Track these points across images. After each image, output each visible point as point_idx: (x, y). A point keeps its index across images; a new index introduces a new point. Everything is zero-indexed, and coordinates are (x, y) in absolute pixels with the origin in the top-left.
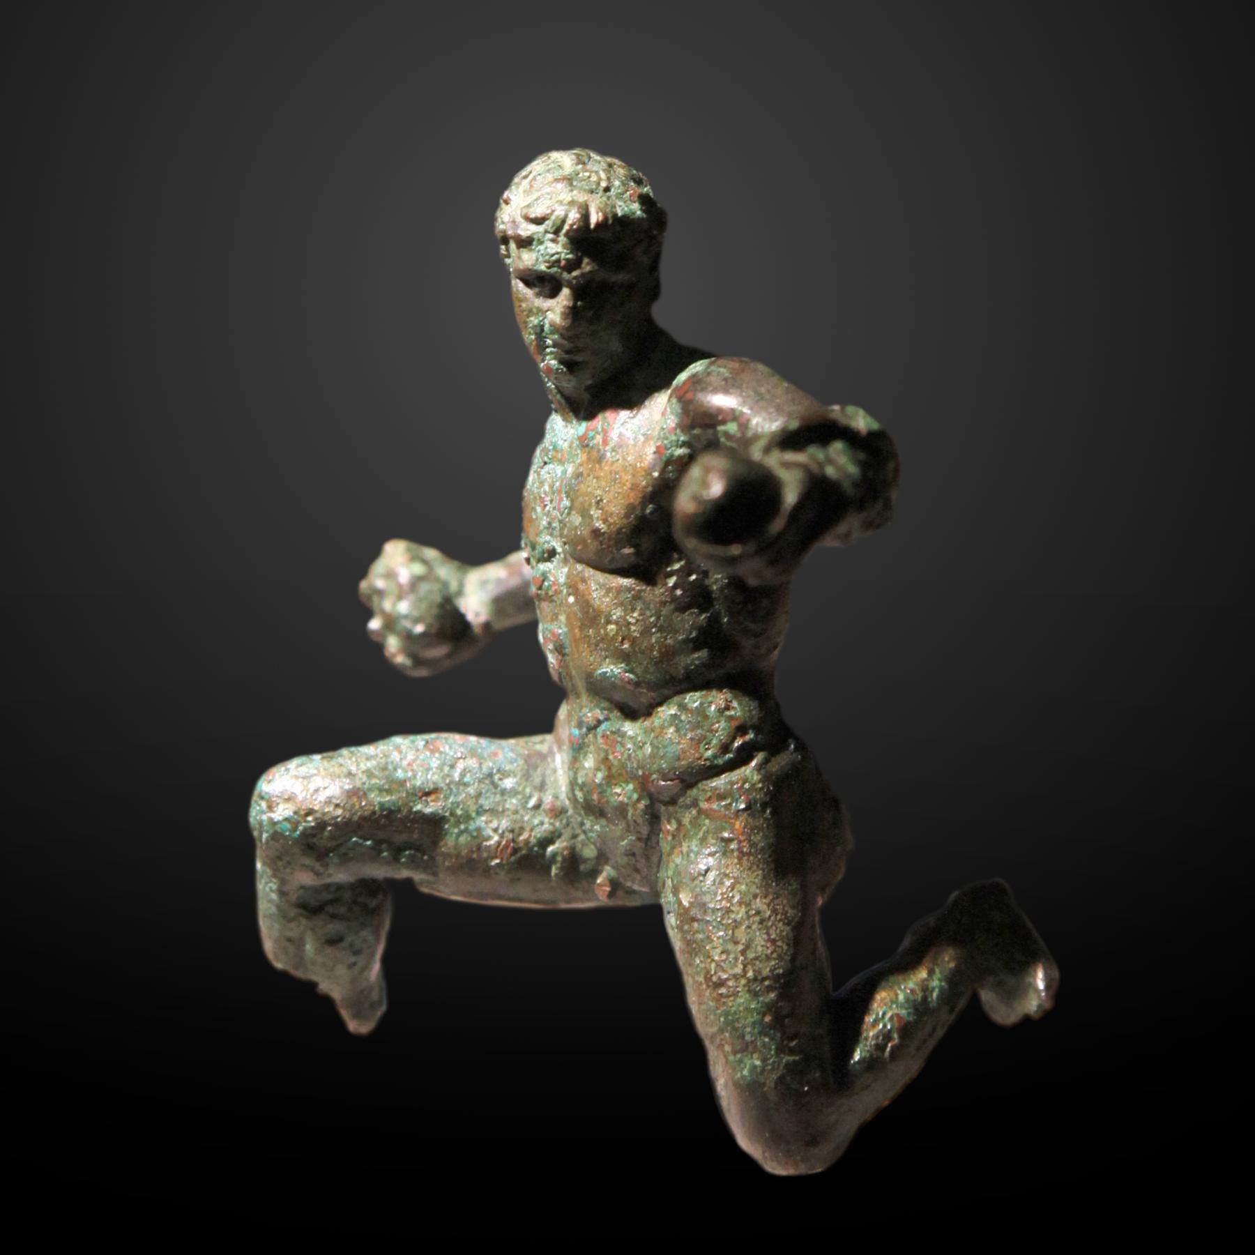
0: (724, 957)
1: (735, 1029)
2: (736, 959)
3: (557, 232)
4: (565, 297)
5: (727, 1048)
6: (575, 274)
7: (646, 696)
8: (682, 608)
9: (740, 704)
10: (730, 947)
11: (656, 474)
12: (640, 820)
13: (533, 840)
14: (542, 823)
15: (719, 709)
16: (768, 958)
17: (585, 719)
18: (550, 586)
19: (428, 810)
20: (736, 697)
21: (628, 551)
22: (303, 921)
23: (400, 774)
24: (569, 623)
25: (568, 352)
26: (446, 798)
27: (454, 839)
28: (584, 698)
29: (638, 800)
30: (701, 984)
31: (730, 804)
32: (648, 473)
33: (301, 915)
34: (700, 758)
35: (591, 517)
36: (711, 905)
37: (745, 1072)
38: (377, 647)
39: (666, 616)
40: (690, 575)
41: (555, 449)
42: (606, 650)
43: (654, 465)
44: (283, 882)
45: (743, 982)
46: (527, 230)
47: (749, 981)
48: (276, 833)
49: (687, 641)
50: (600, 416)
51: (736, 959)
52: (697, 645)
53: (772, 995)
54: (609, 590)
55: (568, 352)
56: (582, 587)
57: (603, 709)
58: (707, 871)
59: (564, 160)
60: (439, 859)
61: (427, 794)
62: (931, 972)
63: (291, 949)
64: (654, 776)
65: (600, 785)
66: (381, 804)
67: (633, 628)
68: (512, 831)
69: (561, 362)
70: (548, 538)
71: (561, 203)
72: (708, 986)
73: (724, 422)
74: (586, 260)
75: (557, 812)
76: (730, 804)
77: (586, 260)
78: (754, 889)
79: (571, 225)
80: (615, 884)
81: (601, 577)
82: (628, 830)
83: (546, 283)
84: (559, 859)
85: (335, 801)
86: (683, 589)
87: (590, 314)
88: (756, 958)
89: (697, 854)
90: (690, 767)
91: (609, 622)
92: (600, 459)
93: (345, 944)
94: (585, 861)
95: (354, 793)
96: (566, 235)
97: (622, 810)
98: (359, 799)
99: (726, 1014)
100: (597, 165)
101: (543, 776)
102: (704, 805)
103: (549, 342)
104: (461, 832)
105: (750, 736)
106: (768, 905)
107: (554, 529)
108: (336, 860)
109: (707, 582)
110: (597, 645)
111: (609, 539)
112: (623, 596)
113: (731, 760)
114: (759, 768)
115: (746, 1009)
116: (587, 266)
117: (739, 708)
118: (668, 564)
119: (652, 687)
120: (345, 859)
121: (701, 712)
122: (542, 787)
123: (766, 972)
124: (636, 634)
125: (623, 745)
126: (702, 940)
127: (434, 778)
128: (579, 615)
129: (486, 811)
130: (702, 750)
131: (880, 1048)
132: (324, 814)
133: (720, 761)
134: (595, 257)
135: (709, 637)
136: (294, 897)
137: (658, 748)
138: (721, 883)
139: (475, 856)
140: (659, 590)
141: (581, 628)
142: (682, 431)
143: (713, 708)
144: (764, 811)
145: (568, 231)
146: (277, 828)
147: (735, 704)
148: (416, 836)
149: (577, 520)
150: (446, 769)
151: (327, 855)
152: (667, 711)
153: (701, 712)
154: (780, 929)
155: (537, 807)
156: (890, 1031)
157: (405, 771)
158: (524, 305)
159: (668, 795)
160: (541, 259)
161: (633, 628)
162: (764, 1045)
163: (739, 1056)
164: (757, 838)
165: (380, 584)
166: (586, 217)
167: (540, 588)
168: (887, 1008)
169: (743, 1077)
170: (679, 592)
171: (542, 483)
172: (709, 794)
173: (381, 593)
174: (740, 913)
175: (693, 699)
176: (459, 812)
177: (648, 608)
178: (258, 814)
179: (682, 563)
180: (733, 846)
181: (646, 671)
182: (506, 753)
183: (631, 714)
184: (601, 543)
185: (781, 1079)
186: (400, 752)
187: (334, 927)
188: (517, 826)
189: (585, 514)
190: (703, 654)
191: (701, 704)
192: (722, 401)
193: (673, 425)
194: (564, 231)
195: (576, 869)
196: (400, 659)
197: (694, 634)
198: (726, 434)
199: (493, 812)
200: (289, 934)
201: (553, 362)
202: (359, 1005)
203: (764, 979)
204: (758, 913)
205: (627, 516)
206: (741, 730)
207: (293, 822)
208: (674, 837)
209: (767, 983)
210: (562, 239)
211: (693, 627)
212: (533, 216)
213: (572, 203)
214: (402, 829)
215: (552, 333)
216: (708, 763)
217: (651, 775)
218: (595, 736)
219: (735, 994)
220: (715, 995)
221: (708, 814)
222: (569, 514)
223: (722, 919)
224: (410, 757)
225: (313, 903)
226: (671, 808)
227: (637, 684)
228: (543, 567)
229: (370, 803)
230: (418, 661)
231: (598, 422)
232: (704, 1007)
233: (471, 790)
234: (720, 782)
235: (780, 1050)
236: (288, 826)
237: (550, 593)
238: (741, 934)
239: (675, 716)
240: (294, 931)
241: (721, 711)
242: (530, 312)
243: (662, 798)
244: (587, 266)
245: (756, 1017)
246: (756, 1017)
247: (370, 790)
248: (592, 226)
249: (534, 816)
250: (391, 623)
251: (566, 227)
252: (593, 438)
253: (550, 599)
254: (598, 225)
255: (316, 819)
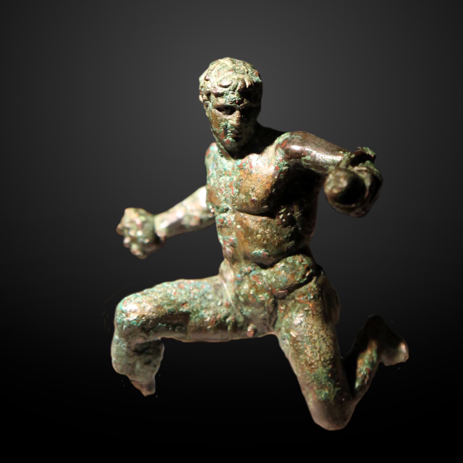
0: (312, 354)
1: (318, 380)
2: (317, 354)
3: (234, 90)
4: (237, 114)
5: (315, 388)
6: (241, 105)
7: (273, 259)
8: (285, 226)
9: (306, 259)
10: (314, 350)
11: (276, 177)
12: (270, 306)
13: (222, 317)
14: (224, 311)
15: (299, 261)
16: (328, 353)
17: (243, 270)
18: (227, 222)
19: (184, 310)
20: (304, 257)
21: (266, 207)
22: (136, 357)
23: (173, 298)
24: (237, 235)
25: (237, 134)
26: (190, 305)
27: (194, 320)
28: (243, 263)
29: (270, 299)
30: (303, 365)
31: (307, 297)
32: (273, 176)
33: (135, 355)
34: (295, 281)
35: (250, 196)
36: (305, 335)
37: (323, 396)
38: (128, 250)
39: (280, 230)
40: (287, 213)
41: (225, 170)
42: (256, 244)
43: (275, 174)
44: (129, 343)
45: (320, 362)
46: (220, 90)
47: (322, 362)
48: (130, 325)
49: (287, 238)
50: (247, 157)
51: (317, 354)
52: (290, 239)
53: (330, 366)
54: (257, 222)
55: (237, 134)
56: (244, 221)
57: (252, 266)
58: (301, 322)
59: (226, 62)
60: (188, 328)
61: (183, 304)
62: (372, 352)
63: (130, 368)
64: (277, 290)
65: (253, 295)
66: (169, 310)
67: (267, 235)
68: (214, 315)
69: (233, 138)
70: (225, 204)
71: (234, 79)
72: (307, 366)
73: (304, 156)
74: (245, 100)
75: (228, 306)
76: (307, 297)
77: (245, 100)
78: (319, 328)
79: (240, 87)
80: (255, 331)
81: (253, 217)
82: (265, 310)
83: (228, 110)
84: (231, 323)
85: (152, 311)
86: (285, 219)
87: (246, 119)
88: (324, 353)
89: (295, 317)
90: (292, 284)
91: (257, 234)
92: (250, 173)
93: (152, 364)
94: (240, 323)
95: (159, 307)
96: (238, 91)
97: (262, 303)
98: (161, 309)
99: (315, 375)
100: (241, 65)
101: (222, 293)
102: (297, 298)
103: (229, 131)
104: (196, 317)
105: (311, 271)
106: (325, 333)
107: (228, 200)
108: (153, 333)
109: (294, 215)
110: (252, 243)
111: (259, 203)
112: (263, 224)
113: (306, 281)
114: (316, 282)
115: (322, 373)
116: (245, 102)
117: (306, 262)
118: (280, 210)
119: (275, 256)
120: (156, 332)
121: (293, 263)
122: (222, 297)
123: (328, 358)
124: (269, 237)
125: (262, 279)
126: (303, 349)
127: (185, 298)
128: (244, 232)
129: (204, 308)
130: (295, 278)
131: (363, 381)
132: (149, 316)
133: (302, 282)
134: (248, 99)
135: (295, 236)
136: (133, 348)
137: (278, 279)
138: (307, 327)
139: (202, 326)
140: (276, 220)
141: (245, 237)
142: (286, 160)
143: (297, 262)
144: (319, 298)
145: (239, 90)
146: (131, 323)
147: (304, 260)
148: (180, 320)
149: (243, 197)
150: (188, 294)
151: (149, 331)
152: (280, 265)
153: (293, 263)
154: (329, 342)
155: (221, 305)
156: (366, 374)
157: (174, 296)
158: (219, 118)
159: (281, 297)
160: (227, 101)
161: (267, 235)
162: (329, 385)
163: (320, 390)
164: (318, 309)
165: (128, 225)
166: (245, 84)
167: (223, 223)
168: (364, 365)
169: (322, 398)
170: (284, 220)
171: (220, 184)
172: (299, 294)
173: (128, 229)
174: (316, 337)
175: (290, 259)
176: (195, 310)
177: (273, 227)
178: (118, 318)
179: (285, 209)
180: (310, 312)
181: (273, 250)
182: (205, 284)
183: (264, 267)
184: (255, 205)
185: (335, 398)
186: (170, 289)
187: (148, 358)
188: (215, 313)
189: (247, 194)
190: (293, 242)
191: (293, 261)
192: (296, 148)
193: (282, 158)
194: (237, 89)
195: (236, 327)
196: (138, 253)
197: (290, 235)
198: (306, 160)
199: (207, 308)
200: (130, 362)
201: (231, 139)
202: (149, 387)
203: (327, 361)
204: (322, 336)
205: (265, 194)
206: (308, 269)
207: (137, 320)
208: (284, 311)
209: (328, 362)
210: (236, 93)
211: (289, 233)
212: (224, 85)
213: (238, 79)
214: (175, 318)
215: (231, 128)
216: (298, 283)
217: (275, 288)
218: (249, 277)
219: (318, 368)
220: (310, 369)
221: (299, 302)
222: (238, 195)
223: (310, 340)
224: (174, 291)
225: (140, 349)
226: (283, 301)
227: (269, 256)
228: (224, 215)
229: (165, 310)
230: (144, 252)
231: (246, 159)
232: (304, 374)
233: (198, 301)
234: (303, 289)
235: (335, 386)
236: (135, 322)
237: (227, 225)
238: (317, 345)
239: (284, 267)
240: (131, 361)
241: (300, 263)
242: (221, 121)
243: (279, 297)
244: (245, 102)
245: (326, 375)
246: (326, 375)
247: (164, 305)
248: (247, 87)
249: (221, 309)
250: (134, 240)
251: (238, 88)
252: (245, 166)
253: (226, 227)
254: (249, 86)
255: (146, 318)
